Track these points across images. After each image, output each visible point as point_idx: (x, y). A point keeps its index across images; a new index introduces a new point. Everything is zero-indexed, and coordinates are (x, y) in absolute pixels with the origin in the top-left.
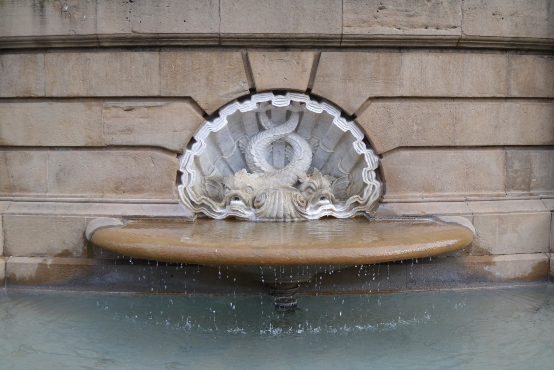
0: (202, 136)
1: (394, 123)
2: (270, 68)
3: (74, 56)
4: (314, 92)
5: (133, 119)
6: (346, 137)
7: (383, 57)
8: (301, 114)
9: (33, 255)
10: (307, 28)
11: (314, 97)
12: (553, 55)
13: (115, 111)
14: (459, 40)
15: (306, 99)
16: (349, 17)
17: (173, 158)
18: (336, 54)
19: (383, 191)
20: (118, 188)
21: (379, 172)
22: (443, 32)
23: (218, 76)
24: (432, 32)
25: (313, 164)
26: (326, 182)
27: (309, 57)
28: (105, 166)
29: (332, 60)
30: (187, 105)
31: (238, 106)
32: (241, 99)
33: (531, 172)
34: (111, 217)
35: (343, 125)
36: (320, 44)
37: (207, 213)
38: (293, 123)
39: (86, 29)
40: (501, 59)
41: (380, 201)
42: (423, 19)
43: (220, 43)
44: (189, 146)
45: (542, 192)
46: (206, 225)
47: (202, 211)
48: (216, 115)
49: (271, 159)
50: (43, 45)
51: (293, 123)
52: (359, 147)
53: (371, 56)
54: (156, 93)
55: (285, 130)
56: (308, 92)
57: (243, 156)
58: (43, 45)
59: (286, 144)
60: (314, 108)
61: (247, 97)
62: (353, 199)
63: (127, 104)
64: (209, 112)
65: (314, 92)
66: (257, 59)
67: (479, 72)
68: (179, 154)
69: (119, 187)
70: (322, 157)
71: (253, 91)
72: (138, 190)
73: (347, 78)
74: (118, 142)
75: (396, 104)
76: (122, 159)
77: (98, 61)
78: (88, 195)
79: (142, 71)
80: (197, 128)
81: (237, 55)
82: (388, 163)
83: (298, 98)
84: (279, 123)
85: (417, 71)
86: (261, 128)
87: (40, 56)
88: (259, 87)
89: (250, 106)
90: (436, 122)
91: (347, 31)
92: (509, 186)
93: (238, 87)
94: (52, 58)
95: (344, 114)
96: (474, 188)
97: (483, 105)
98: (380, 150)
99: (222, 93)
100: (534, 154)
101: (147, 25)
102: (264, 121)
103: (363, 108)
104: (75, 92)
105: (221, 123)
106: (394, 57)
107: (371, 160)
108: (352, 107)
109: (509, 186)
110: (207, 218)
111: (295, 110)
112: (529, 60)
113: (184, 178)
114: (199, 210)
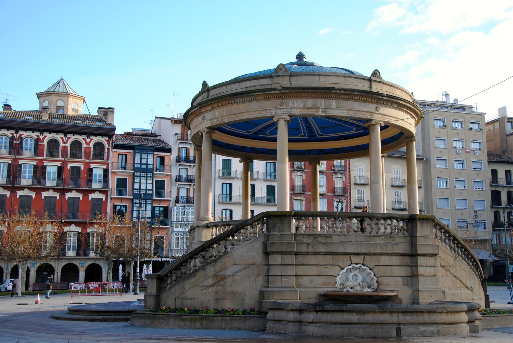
0: (341, 273)
1: (380, 271)
3: (314, 256)
7: (377, 257)
10: (363, 251)
11: (364, 265)
13: (323, 268)
15: (362, 265)
16: (371, 249)
18: (368, 256)
19: (378, 285)
20: (323, 285)
21: (377, 282)
24: (387, 252)
27: (363, 257)
28: (321, 280)
29: (367, 258)
30: (338, 267)
31: (348, 267)
36: (365, 254)
39: (318, 251)
40: (400, 257)
41: (378, 288)
42: (385, 249)
43: (345, 254)
47: (101, 264)
50: (307, 254)
51: (358, 270)
53: (375, 257)
55: (356, 272)
58: (307, 254)
59: (356, 275)
60: (364, 267)
62: (372, 287)
67: (396, 260)
68: (336, 277)
69: (324, 284)
71: (352, 264)
72: (328, 285)
73: (370, 261)
75: (380, 267)
77: (319, 257)
78: (317, 286)
79: (329, 259)
81: (348, 256)
82: (379, 279)
83: (361, 265)
85: (384, 260)
87: (306, 256)
88: (373, 270)
89: (350, 267)
90: (183, 186)
92: (404, 285)
94: (309, 256)
97: (397, 267)
100: (409, 278)
101: (330, 250)
103: (374, 268)
104: (314, 263)
105: (345, 271)
106: (379, 257)
108: (372, 267)
109: (404, 285)
112: (406, 257)
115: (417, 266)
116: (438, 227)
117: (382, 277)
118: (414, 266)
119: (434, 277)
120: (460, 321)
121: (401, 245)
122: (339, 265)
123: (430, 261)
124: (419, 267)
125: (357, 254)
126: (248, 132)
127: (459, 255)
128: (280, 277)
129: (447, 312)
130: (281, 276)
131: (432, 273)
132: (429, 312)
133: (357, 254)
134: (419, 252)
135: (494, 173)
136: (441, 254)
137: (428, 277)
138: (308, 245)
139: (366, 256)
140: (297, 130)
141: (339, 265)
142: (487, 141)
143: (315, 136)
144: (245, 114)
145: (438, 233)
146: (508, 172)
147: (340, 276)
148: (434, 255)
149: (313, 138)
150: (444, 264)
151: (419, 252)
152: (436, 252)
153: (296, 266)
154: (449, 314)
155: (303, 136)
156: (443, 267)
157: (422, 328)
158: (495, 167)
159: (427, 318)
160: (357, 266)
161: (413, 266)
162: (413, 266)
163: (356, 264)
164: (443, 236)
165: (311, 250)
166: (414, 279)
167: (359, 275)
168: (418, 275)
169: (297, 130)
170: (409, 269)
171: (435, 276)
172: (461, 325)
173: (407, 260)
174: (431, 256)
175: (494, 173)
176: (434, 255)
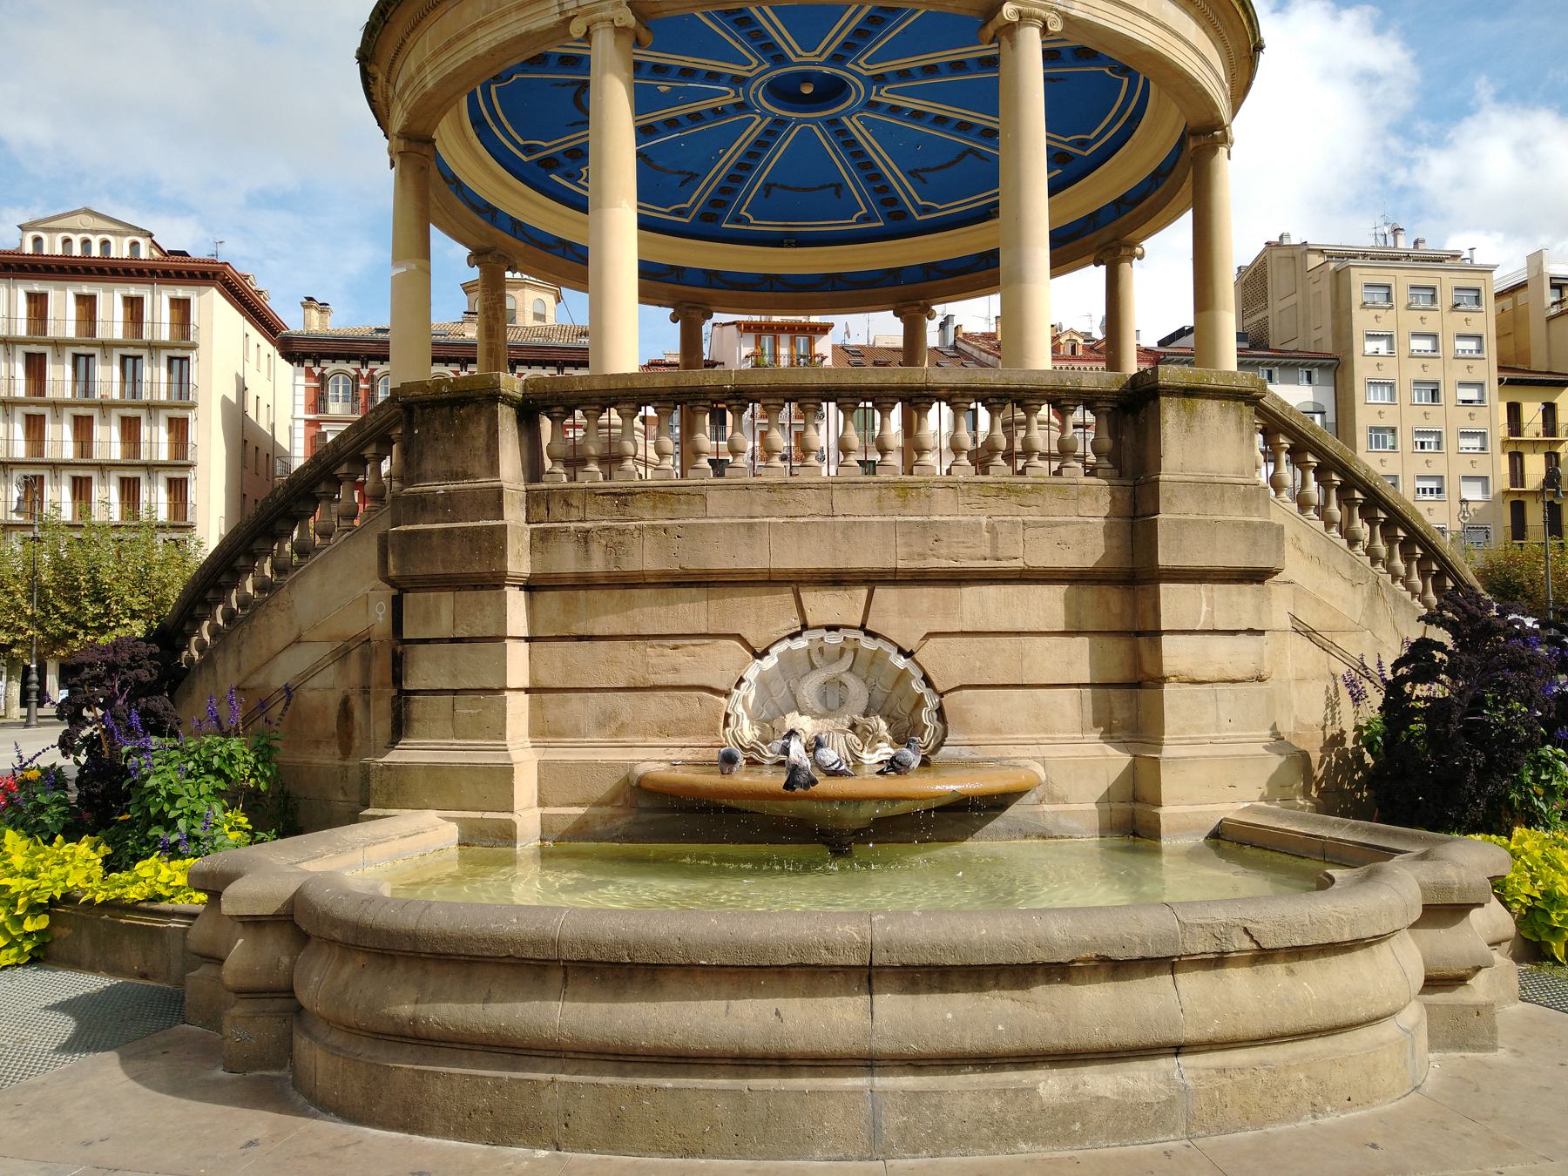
2: (824, 605)
4: (868, 627)
5: (679, 657)
6: (903, 675)
8: (856, 651)
9: (580, 805)
12: (1567, 103)
14: (1023, 571)
15: (860, 635)
16: (902, 551)
17: (722, 699)
21: (940, 711)
22: (1004, 564)
23: (767, 615)
25: (869, 706)
26: (883, 725)
27: (863, 592)
29: (887, 597)
31: (787, 644)
32: (792, 637)
33: (1111, 712)
34: (658, 759)
35: (901, 662)
36: (872, 579)
37: (756, 757)
38: (848, 660)
43: (771, 581)
44: (737, 686)
45: (1124, 736)
46: (756, 769)
48: (766, 652)
49: (823, 698)
52: (918, 687)
54: (704, 631)
56: (862, 627)
57: (794, 697)
60: (868, 644)
61: (798, 634)
63: (672, 643)
64: (759, 651)
65: (868, 627)
66: (810, 598)
67: (1048, 604)
70: (879, 697)
71: (805, 627)
74: (664, 682)
76: (666, 700)
79: (691, 612)
80: (744, 666)
83: (852, 635)
84: (832, 662)
85: (979, 605)
86: (813, 667)
88: (811, 623)
89: (801, 643)
90: (999, 660)
91: (901, 565)
93: (789, 624)
94: (595, 595)
95: (901, 651)
96: (1046, 731)
98: (941, 688)
99: (772, 629)
102: (816, 659)
105: (769, 662)
107: (931, 702)
110: (757, 763)
111: (849, 647)
113: (731, 720)
114: (750, 754)
115: (1159, 633)
116: (1284, 441)
117: (965, 692)
118: (1143, 633)
119: (1256, 686)
120: (1362, 1014)
121: (1079, 528)
122: (739, 637)
123: (1236, 603)
124: (1166, 640)
125: (837, 580)
126: (679, 213)
127: (1395, 578)
128: (448, 698)
129: (1263, 956)
130: (455, 692)
131: (1243, 668)
132: (1115, 968)
133: (837, 580)
134: (1164, 559)
135: (1514, 410)
136: (1294, 566)
137: (1220, 687)
138: (585, 537)
139: (878, 591)
140: (837, 193)
141: (739, 637)
142: (1498, 338)
143: (903, 214)
144: (480, 33)
145: (1287, 472)
146: (1549, 410)
147: (749, 692)
148: (1257, 576)
149: (900, 226)
150: (1310, 618)
151: (1164, 559)
152: (1262, 562)
153: (535, 644)
154: (1278, 969)
155: (865, 219)
156: (1309, 633)
157: (1050, 1084)
158: (1515, 395)
159: (1093, 1008)
160: (834, 639)
161: (1138, 634)
162: (1138, 634)
163: (830, 628)
164: (1313, 485)
165: (598, 564)
166: (1143, 694)
167: (850, 680)
168: (1160, 681)
169: (837, 193)
170: (1117, 650)
171: (1260, 679)
172: (1365, 1034)
173: (1114, 597)
174: (1228, 581)
175: (1514, 410)
176: (1257, 576)
